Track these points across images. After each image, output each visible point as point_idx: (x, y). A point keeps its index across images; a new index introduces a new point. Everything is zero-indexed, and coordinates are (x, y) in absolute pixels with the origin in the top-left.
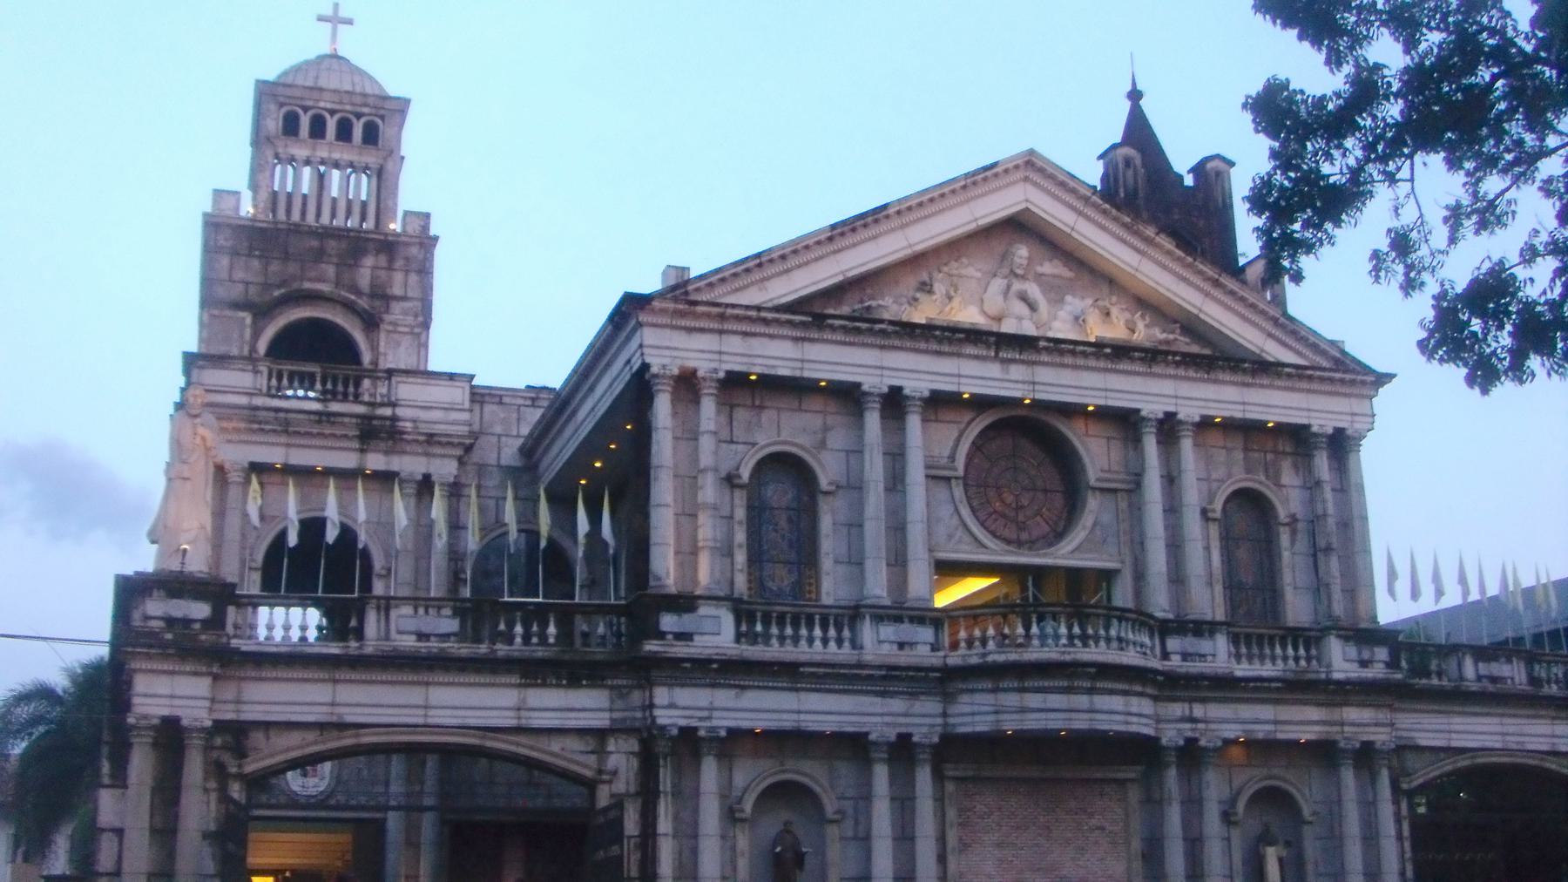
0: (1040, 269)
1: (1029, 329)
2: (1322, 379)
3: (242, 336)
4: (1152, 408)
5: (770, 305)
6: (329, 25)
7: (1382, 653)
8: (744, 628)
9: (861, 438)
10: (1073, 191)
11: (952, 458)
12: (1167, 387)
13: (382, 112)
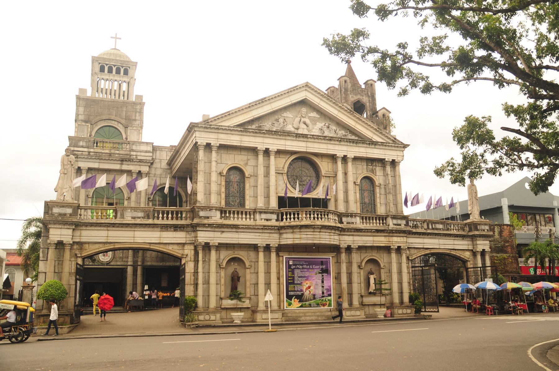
0: (310, 115)
1: (306, 132)
2: (389, 146)
3: (88, 130)
4: (340, 154)
5: (232, 126)
6: (115, 39)
7: (404, 222)
8: (223, 215)
9: (257, 162)
10: (319, 93)
11: (283, 168)
12: (345, 148)
13: (129, 66)
